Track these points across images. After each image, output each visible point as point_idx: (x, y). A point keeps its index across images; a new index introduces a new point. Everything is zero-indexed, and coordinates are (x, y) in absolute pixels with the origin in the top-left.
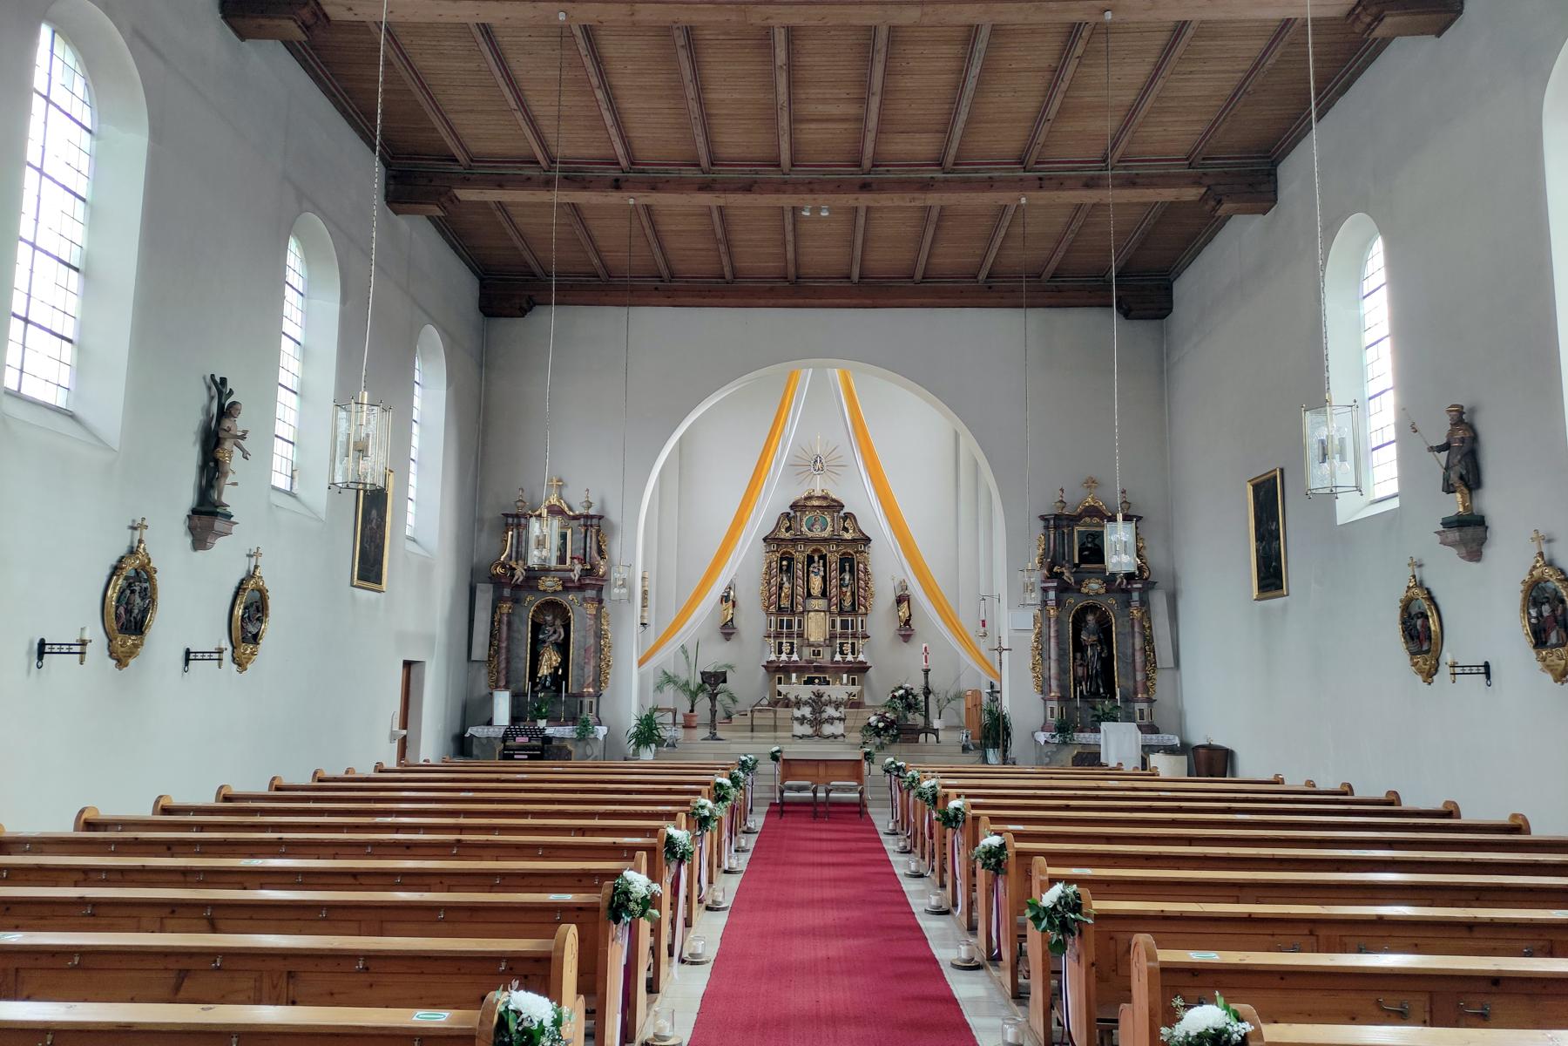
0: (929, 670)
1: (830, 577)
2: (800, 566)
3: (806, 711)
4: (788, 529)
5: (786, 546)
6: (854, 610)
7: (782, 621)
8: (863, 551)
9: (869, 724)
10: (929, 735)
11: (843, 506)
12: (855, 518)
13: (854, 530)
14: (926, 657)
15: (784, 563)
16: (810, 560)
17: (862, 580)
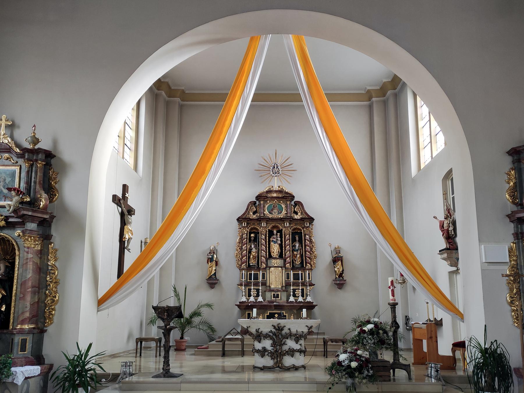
0: (397, 304)
1: (285, 244)
2: (263, 237)
3: (267, 344)
4: (254, 213)
5: (254, 224)
6: (302, 267)
7: (251, 274)
8: (308, 227)
9: (340, 363)
10: (396, 370)
11: (294, 197)
12: (302, 205)
13: (302, 213)
14: (393, 291)
15: (252, 235)
16: (271, 233)
17: (308, 246)
